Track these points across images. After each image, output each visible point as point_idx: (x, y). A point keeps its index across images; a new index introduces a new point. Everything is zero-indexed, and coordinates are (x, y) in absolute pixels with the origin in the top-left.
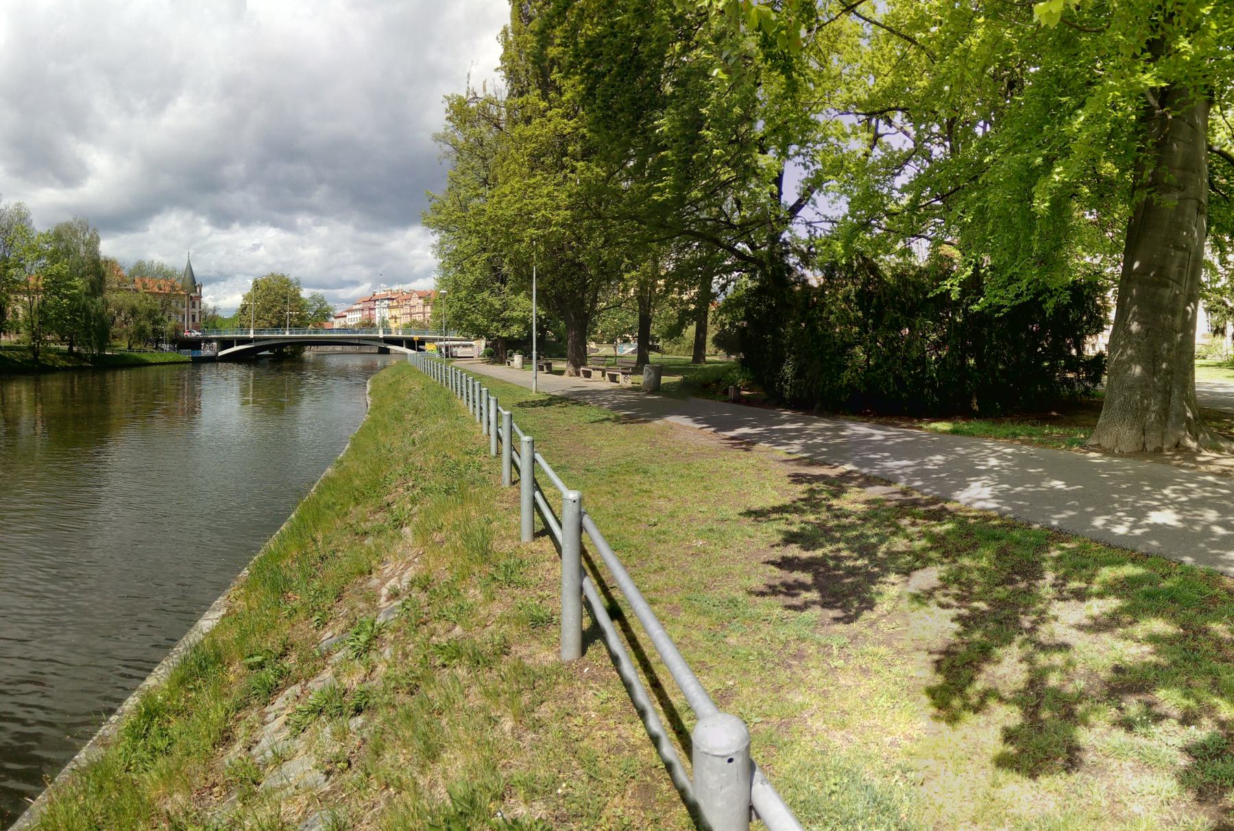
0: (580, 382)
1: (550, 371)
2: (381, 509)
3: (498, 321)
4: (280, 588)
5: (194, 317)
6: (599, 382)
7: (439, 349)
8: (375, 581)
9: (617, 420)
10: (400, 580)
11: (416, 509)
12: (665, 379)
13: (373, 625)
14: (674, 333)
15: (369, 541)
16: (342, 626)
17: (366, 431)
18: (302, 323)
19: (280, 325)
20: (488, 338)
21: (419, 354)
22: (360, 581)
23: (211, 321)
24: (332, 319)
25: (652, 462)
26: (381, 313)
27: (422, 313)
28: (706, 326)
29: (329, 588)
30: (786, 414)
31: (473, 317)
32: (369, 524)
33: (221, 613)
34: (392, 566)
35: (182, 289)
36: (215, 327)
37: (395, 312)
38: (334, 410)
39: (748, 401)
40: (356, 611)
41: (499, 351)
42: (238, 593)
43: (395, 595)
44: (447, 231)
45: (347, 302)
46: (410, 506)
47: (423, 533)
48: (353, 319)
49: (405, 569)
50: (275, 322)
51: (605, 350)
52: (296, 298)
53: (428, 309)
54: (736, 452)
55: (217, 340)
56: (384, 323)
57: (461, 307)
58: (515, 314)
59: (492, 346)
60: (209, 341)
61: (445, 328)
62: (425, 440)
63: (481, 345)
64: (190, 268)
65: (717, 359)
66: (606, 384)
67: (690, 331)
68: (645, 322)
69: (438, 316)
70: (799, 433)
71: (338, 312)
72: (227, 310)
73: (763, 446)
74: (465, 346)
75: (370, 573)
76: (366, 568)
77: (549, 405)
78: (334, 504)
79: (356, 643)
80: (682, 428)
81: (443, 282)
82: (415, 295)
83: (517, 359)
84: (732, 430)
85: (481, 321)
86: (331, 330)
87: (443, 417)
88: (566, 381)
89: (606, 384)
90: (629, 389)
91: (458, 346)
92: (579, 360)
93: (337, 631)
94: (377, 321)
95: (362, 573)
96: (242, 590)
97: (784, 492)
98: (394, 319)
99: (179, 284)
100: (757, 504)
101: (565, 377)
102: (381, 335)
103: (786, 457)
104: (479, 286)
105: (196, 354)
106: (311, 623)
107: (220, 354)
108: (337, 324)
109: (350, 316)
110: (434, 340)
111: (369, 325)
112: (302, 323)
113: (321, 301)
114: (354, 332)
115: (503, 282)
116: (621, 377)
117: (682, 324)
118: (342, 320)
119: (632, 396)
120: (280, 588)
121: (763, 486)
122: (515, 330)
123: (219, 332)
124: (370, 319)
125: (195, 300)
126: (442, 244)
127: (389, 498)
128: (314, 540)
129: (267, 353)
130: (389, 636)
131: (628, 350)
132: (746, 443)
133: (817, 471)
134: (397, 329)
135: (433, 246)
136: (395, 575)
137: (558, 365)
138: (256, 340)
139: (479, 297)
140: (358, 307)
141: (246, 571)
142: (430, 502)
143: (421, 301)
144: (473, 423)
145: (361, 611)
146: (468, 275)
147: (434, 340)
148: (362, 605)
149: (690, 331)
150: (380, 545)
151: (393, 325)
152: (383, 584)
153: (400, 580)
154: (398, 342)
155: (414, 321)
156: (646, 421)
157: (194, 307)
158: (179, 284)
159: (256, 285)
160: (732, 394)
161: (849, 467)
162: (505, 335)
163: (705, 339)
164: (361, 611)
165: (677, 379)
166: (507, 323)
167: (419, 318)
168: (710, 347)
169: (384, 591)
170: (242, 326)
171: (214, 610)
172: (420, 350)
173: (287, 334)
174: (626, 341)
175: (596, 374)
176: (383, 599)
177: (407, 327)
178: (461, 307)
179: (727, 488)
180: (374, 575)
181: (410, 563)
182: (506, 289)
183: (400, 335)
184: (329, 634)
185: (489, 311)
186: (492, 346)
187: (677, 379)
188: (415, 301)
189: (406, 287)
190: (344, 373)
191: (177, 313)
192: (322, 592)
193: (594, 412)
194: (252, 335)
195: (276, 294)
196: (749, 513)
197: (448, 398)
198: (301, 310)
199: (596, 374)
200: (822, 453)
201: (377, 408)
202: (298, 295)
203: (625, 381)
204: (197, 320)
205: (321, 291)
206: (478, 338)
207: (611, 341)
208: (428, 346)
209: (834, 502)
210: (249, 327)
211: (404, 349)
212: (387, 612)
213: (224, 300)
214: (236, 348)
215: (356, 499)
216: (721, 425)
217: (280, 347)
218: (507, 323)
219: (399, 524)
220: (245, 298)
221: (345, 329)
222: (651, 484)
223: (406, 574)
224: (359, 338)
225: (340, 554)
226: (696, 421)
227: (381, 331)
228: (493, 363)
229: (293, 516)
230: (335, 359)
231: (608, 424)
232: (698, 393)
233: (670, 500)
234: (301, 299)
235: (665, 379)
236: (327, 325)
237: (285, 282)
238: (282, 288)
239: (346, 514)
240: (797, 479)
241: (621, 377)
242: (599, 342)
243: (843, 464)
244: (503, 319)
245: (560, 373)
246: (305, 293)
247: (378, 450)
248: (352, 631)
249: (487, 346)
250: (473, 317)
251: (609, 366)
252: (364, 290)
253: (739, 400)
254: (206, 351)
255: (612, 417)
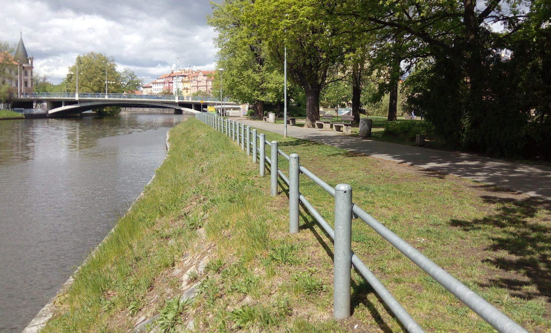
0: (316, 131)
1: (294, 124)
2: (180, 217)
3: (258, 90)
4: (101, 289)
5: (26, 83)
6: (328, 131)
7: (217, 110)
8: (177, 271)
9: (347, 155)
10: (197, 268)
11: (207, 215)
12: (373, 130)
13: (178, 304)
14: (376, 98)
15: (171, 242)
16: (153, 310)
17: (166, 165)
18: (118, 89)
19: (100, 90)
20: (251, 103)
21: (204, 114)
22: (166, 272)
23: (44, 86)
24: (142, 89)
25: (370, 183)
26: (177, 85)
27: (206, 85)
28: (397, 96)
29: (142, 281)
30: (464, 155)
31: (241, 87)
32: (171, 230)
33: (47, 319)
34: (190, 258)
35: (15, 60)
36: (45, 91)
37: (187, 85)
38: (144, 151)
39: (430, 146)
40: (164, 295)
41: (259, 110)
42: (63, 298)
43: (194, 279)
44: (225, 29)
45: (153, 76)
46: (202, 213)
47: (213, 230)
48: (158, 89)
49: (201, 258)
50: (96, 88)
51: (330, 112)
52: (112, 70)
53: (210, 83)
54: (432, 179)
55: (47, 100)
56: (179, 92)
57: (233, 80)
58: (270, 86)
59: (253, 108)
60: (40, 101)
61: (221, 96)
62: (210, 168)
63: (245, 108)
64: (22, 44)
65: (403, 118)
66: (334, 132)
67: (386, 98)
68: (357, 92)
69: (217, 87)
70: (479, 168)
71: (145, 84)
72: (58, 78)
73: (451, 175)
74: (235, 109)
75: (173, 265)
76: (170, 262)
77: (297, 144)
78: (144, 218)
79: (165, 321)
80: (386, 162)
81: (221, 64)
82: (201, 74)
83: (272, 116)
84: (424, 164)
85: (246, 90)
86: (141, 96)
87: (223, 152)
88: (305, 129)
89: (334, 132)
90: (349, 135)
91: (230, 109)
92: (315, 117)
93: (149, 315)
94: (174, 91)
95: (167, 266)
96: (67, 296)
97: (480, 209)
98: (186, 91)
99: (12, 56)
100: (461, 216)
101: (305, 128)
102: (177, 100)
103: (472, 184)
104: (246, 66)
105: (28, 111)
106: (127, 312)
107: (51, 112)
108: (145, 92)
109: (154, 87)
110: (213, 104)
111: (168, 93)
112: (118, 89)
113: (132, 75)
114: (158, 98)
115: (261, 63)
116: (344, 128)
117: (381, 93)
118: (149, 90)
119: (353, 139)
120: (101, 289)
121: (461, 203)
122: (270, 97)
123: (48, 94)
124: (169, 90)
125: (27, 70)
126: (221, 38)
127: (186, 210)
128: (131, 247)
129: (90, 112)
130: (191, 311)
131: (345, 112)
132: (441, 174)
133: (504, 195)
134: (188, 97)
135: (215, 39)
136: (193, 263)
137: (299, 121)
138: (80, 101)
139: (245, 74)
140: (161, 81)
141: (71, 279)
142: (216, 210)
143: (206, 78)
144: (245, 156)
145: (169, 295)
146: (238, 58)
147: (213, 104)
148: (169, 291)
149: (386, 98)
150: (180, 243)
151: (185, 94)
152: (183, 272)
153: (197, 268)
154: (189, 105)
155: (200, 91)
156: (365, 155)
157: (26, 74)
158: (12, 56)
159: (80, 61)
160: (418, 140)
161: (532, 194)
162: (263, 99)
163: (396, 104)
164: (169, 295)
165: (382, 129)
166: (263, 91)
167: (203, 89)
168: (399, 111)
169: (186, 277)
170: (68, 91)
171: (41, 316)
172: (204, 111)
173: (106, 98)
174: (343, 106)
175: (327, 126)
176: (184, 283)
177: (195, 96)
178: (233, 80)
179: (433, 203)
180: (176, 267)
181: (204, 254)
182: (264, 69)
183: (190, 100)
184: (143, 318)
185: (252, 84)
186: (253, 108)
187: (382, 129)
188: (200, 77)
189: (195, 68)
190: (152, 126)
191: (11, 79)
192: (137, 285)
193: (328, 149)
194: (77, 98)
195: (96, 68)
196: (455, 223)
197: (226, 140)
198: (117, 81)
199: (327, 126)
200: (505, 183)
201: (174, 150)
202: (114, 69)
203: (347, 131)
204: (29, 85)
205: (132, 68)
206: (244, 102)
207: (333, 106)
208: (209, 109)
209: (528, 219)
210: (75, 91)
211: (193, 111)
212: (189, 293)
213: (53, 71)
214: (63, 108)
215: (161, 212)
216: (416, 161)
217: (99, 107)
218: (263, 91)
219: (194, 227)
220: (71, 70)
221: (151, 96)
222: (373, 197)
223: (202, 262)
224: (162, 103)
225: (151, 254)
226: (394, 158)
227: (177, 98)
228: (254, 119)
229: (113, 230)
230: (144, 116)
231: (340, 157)
232: (394, 138)
233: (390, 209)
234: (116, 73)
235: (373, 130)
236: (137, 93)
237: (102, 59)
238: (100, 63)
239: (154, 224)
240: (488, 200)
241: (344, 128)
242: (325, 107)
243: (526, 191)
244: (262, 89)
245: (302, 125)
246: (120, 68)
247: (176, 178)
248: (162, 312)
249: (249, 109)
250: (241, 87)
251: (332, 121)
252: (165, 70)
253: (423, 145)
254: (38, 110)
255: (342, 152)
